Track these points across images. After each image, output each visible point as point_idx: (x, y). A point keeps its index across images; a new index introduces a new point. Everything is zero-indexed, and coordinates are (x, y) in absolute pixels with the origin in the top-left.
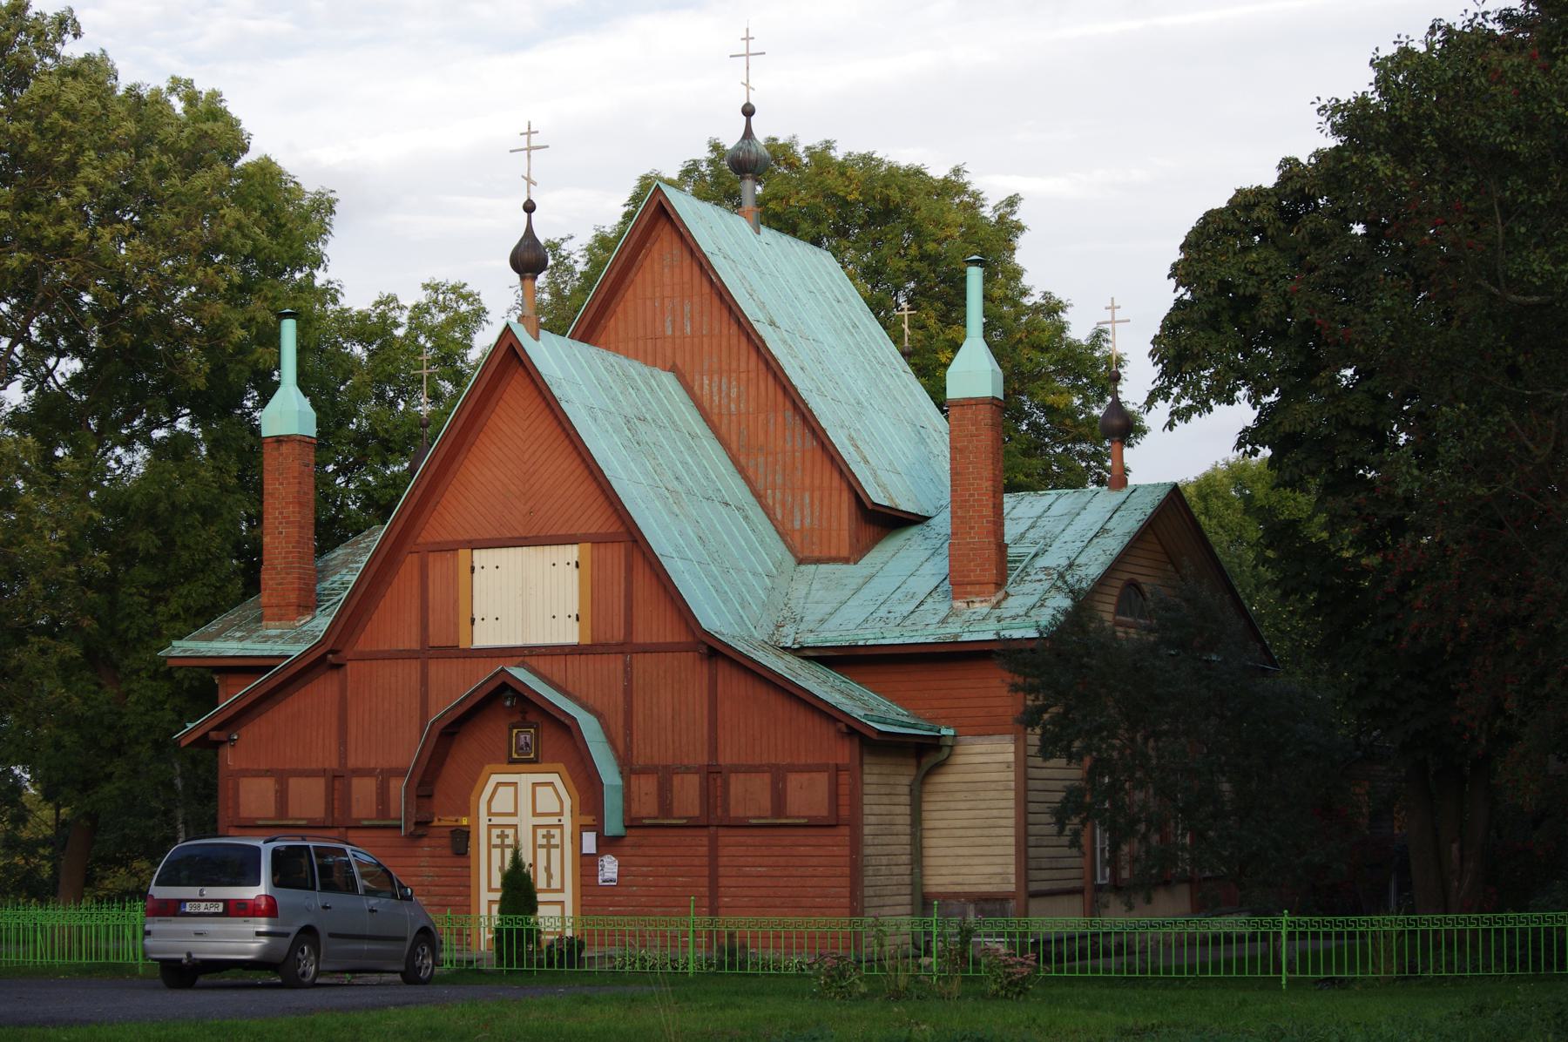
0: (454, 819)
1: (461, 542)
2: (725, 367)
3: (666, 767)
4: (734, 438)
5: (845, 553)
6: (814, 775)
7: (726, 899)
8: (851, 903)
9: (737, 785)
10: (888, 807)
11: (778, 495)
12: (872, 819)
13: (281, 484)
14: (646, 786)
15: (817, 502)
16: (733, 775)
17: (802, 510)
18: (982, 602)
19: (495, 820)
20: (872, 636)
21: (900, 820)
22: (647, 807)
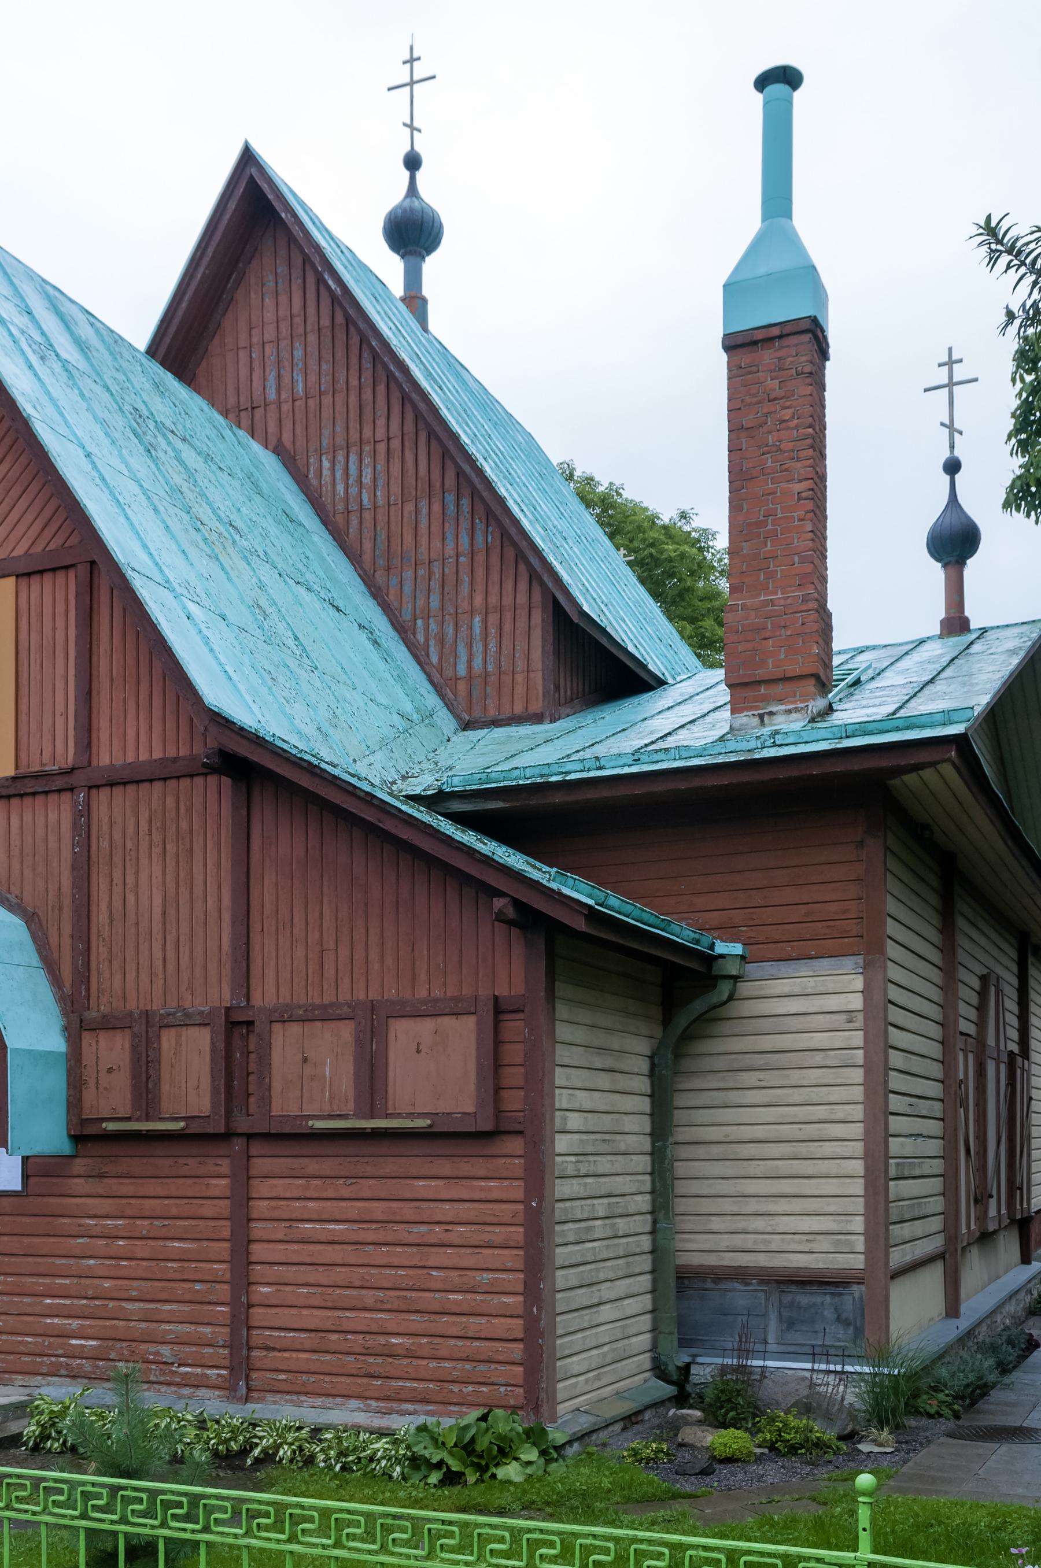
2: (354, 437)
3: (147, 1015)
4: (367, 545)
5: (537, 706)
6: (447, 1022)
7: (265, 1289)
8: (528, 1305)
11: (433, 626)
12: (575, 1121)
15: (493, 631)
16: (277, 1027)
17: (470, 646)
18: (789, 712)
20: (579, 767)
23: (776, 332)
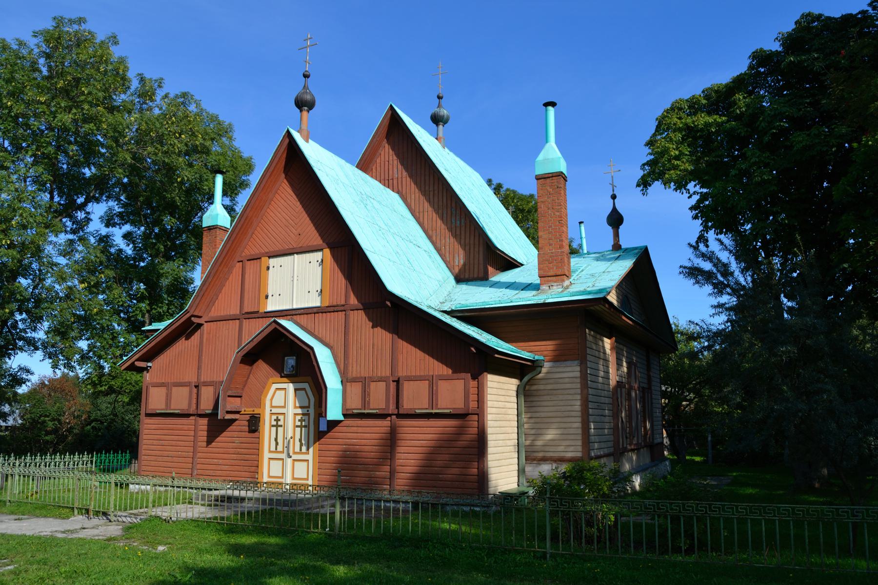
0: (252, 409)
1: (263, 253)
9: (408, 389)
10: (503, 403)
13: (209, 249)
14: (356, 390)
18: (557, 285)
19: (274, 411)
21: (510, 411)
22: (356, 405)
23: (551, 175)
